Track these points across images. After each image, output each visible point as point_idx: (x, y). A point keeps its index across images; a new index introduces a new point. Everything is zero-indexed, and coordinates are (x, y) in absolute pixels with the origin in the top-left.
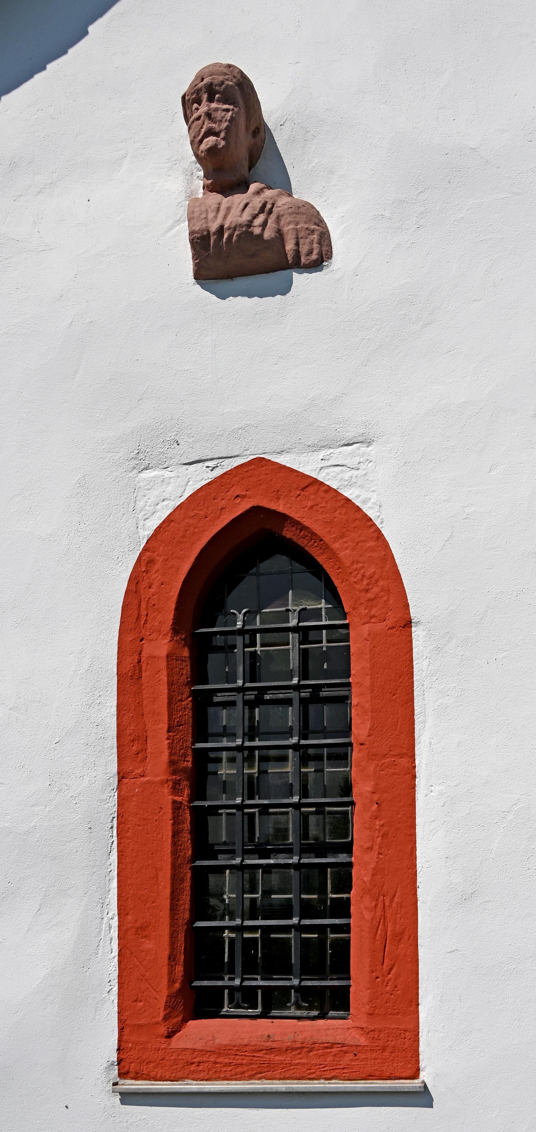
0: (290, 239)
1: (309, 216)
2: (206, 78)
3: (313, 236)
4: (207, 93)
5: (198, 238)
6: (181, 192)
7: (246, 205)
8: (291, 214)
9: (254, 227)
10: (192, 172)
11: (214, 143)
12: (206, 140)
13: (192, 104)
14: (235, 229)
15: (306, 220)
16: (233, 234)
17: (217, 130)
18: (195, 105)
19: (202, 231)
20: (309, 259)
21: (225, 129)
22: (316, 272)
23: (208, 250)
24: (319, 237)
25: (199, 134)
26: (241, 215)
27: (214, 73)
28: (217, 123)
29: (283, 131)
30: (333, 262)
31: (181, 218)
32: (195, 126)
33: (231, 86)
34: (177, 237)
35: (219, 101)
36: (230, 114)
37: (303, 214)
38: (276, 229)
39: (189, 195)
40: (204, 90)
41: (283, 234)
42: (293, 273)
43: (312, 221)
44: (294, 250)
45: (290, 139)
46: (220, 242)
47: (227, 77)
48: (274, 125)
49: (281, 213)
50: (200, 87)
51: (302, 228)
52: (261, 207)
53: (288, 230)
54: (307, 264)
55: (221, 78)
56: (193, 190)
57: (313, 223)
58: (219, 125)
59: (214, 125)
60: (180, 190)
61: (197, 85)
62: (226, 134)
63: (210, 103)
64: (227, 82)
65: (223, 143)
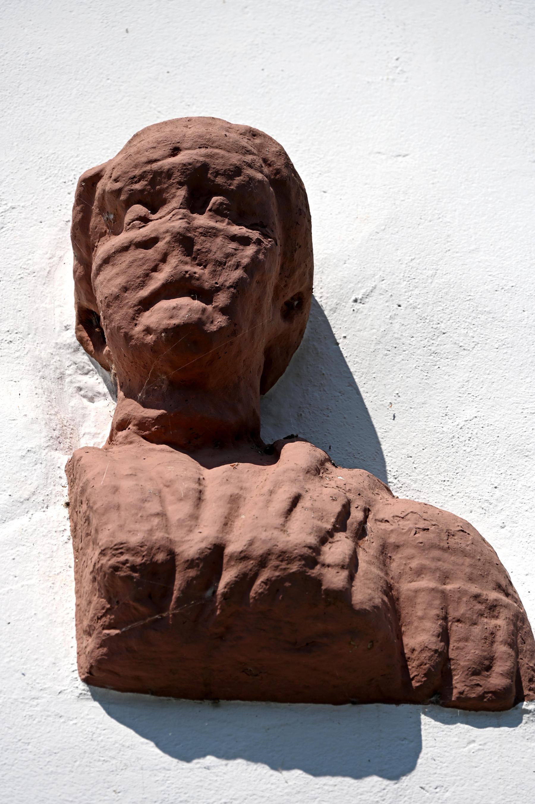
0: (421, 618)
1: (480, 563)
2: (186, 149)
3: (494, 622)
4: (185, 187)
5: (133, 568)
6: (34, 421)
9: (323, 565)
10: (62, 374)
11: (196, 316)
12: (164, 304)
13: (128, 204)
15: (472, 573)
16: (256, 576)
17: (207, 286)
18: (138, 209)
20: (478, 685)
21: (231, 286)
22: (499, 726)
23: (163, 609)
24: (512, 627)
25: (142, 285)
26: (283, 525)
27: (213, 142)
28: (210, 267)
29: (360, 316)
33: (260, 182)
34: (21, 548)
35: (218, 212)
36: (250, 250)
37: (464, 553)
38: (382, 583)
39: (56, 433)
40: (177, 177)
41: (398, 599)
42: (423, 717)
43: (490, 578)
44: (436, 651)
45: (383, 340)
46: (207, 588)
47: (249, 158)
48: (332, 296)
49: (392, 539)
50: (167, 167)
51: (462, 592)
52: (340, 514)
53: (416, 591)
54: (470, 699)
55: (235, 159)
57: (493, 585)
58: (214, 273)
59: (198, 270)
60: (32, 415)
61: (156, 161)
62: (234, 298)
63: (193, 213)
64: (250, 172)
65: (220, 321)
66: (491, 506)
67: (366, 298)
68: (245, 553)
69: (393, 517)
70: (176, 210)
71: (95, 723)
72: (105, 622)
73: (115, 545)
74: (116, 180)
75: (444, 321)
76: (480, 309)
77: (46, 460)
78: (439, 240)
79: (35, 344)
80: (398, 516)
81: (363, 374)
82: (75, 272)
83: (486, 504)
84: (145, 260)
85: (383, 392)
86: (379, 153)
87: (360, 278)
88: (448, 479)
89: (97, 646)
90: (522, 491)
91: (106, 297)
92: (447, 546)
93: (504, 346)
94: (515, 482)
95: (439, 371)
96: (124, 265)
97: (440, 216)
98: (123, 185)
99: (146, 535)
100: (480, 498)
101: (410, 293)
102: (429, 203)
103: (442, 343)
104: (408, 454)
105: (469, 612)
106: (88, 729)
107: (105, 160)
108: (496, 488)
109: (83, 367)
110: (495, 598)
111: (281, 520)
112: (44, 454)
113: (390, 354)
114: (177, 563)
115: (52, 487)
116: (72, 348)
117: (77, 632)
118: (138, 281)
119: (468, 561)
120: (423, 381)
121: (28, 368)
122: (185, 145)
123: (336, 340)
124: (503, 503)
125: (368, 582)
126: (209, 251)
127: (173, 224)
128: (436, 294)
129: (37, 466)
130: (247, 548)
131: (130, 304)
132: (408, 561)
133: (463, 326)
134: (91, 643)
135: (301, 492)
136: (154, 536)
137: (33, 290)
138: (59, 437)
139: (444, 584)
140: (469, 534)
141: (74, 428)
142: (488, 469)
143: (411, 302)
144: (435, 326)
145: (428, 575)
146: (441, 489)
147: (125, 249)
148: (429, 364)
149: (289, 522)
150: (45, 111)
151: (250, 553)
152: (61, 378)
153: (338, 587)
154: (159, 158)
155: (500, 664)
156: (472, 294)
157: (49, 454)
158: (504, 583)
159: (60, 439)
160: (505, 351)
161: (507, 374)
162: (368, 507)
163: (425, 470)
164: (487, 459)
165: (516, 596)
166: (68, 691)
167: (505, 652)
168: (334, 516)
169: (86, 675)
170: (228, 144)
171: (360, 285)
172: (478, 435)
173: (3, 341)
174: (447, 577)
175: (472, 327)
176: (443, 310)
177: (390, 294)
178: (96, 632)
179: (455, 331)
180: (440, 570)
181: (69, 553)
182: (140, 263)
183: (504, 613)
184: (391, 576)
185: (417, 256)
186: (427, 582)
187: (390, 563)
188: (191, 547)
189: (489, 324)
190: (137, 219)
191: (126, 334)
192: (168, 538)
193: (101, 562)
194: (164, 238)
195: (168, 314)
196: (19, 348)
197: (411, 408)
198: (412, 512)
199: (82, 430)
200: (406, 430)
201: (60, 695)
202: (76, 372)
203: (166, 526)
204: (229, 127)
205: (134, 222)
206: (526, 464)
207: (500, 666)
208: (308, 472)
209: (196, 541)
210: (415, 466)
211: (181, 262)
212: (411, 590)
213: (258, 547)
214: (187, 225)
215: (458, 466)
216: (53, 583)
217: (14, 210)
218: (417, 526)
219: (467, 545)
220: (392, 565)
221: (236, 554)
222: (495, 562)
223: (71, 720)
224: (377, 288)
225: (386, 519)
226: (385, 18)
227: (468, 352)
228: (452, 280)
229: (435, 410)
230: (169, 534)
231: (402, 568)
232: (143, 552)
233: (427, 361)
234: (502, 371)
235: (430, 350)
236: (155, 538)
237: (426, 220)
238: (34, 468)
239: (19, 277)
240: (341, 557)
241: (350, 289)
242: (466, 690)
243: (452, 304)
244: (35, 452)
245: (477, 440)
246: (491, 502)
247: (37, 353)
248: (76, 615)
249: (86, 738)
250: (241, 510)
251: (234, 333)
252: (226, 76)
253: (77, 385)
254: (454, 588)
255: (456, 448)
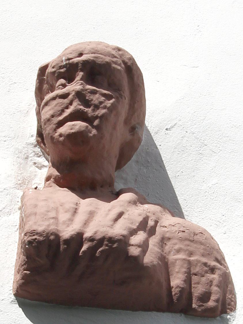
0: (178, 272)
1: (208, 248)
3: (213, 276)
7: (120, 215)
8: (182, 240)
14: (101, 241)
15: (204, 253)
18: (62, 81)
19: (48, 234)
25: (60, 114)
26: (112, 225)
28: (92, 108)
30: (237, 316)
31: (4, 208)
32: (58, 104)
37: (201, 243)
38: (159, 255)
39: (20, 182)
47: (114, 60)
49: (167, 235)
50: (75, 62)
51: (198, 261)
53: (176, 260)
56: (25, 178)
57: (214, 259)
58: (94, 110)
61: (71, 59)
66: (220, 224)
67: (172, 128)
68: (92, 238)
69: (169, 225)
70: (78, 81)
71: (17, 315)
72: (25, 267)
73: (31, 231)
74: (53, 68)
75: (207, 140)
76: (223, 135)
77: (12, 193)
78: (208, 104)
79: (17, 142)
80: (171, 225)
81: (167, 162)
82: (36, 110)
83: (218, 223)
84: (63, 104)
85: (176, 170)
86: (185, 65)
87: (170, 119)
88: (202, 211)
89: (21, 278)
90: (235, 217)
91: (44, 120)
92: (193, 239)
93: (233, 152)
94: (233, 213)
95: (202, 162)
96: (53, 105)
97: (210, 94)
98: (56, 70)
99: (46, 227)
100: (216, 220)
101: (192, 127)
102: (205, 88)
103: (205, 149)
104: (184, 199)
105: (201, 271)
106: (13, 318)
107: (51, 61)
108: (223, 215)
109: (38, 154)
110: (214, 264)
111: (112, 223)
112: (12, 191)
113: (180, 154)
114: (61, 241)
115: (13, 206)
116: (33, 145)
117: (15, 272)
118: (59, 113)
119: (202, 247)
120: (195, 166)
121: (12, 153)
122: (85, 52)
123: (156, 146)
124: (226, 222)
125: (152, 254)
126: (92, 100)
127: (76, 87)
128: (204, 128)
129: (7, 196)
130: (93, 235)
131: (54, 123)
132: (174, 246)
133: (215, 142)
134: (19, 277)
135: (124, 211)
136: (50, 228)
137: (19, 119)
138: (21, 184)
139: (190, 257)
140: (204, 235)
141: (30, 181)
142: (220, 207)
143: (192, 131)
144: (202, 142)
145: (183, 252)
146: (198, 215)
147: (54, 99)
148: (198, 159)
149: (115, 224)
150: (36, 42)
151: (95, 238)
152: (27, 158)
153: (136, 255)
154: (73, 58)
155: (214, 296)
156: (221, 128)
157: (14, 191)
158: (219, 258)
159: (22, 185)
160: (233, 154)
161: (234, 165)
162: (157, 220)
163: (192, 206)
164: (221, 202)
165: (226, 265)
166: (6, 299)
167: (216, 290)
168: (138, 223)
169: (15, 292)
170: (105, 53)
171: (169, 122)
172: (218, 191)
173: (2, 140)
174: (192, 254)
175: (219, 143)
176: (207, 135)
177: (183, 127)
178: (21, 272)
179: (211, 144)
180: (188, 251)
181: (17, 236)
182: (60, 105)
183: (218, 272)
184: (165, 252)
185: (197, 111)
186: (182, 255)
187: (165, 246)
188: (67, 233)
189: (228, 142)
190: (61, 85)
191: (51, 136)
192: (56, 229)
193: (24, 239)
194: (72, 94)
195: (70, 128)
196: (9, 144)
197: (188, 178)
198: (178, 223)
199: (34, 182)
200: (184, 188)
201: (3, 301)
202: (34, 156)
203: (57, 223)
204: (108, 46)
205: (60, 86)
206: (239, 205)
207: (214, 297)
208: (130, 202)
209: (70, 231)
210: (187, 204)
211: (78, 104)
212: (174, 259)
213: (99, 235)
214: (83, 88)
215: (207, 205)
216: (7, 249)
217: (16, 84)
218: (180, 230)
219: (203, 240)
220: (166, 247)
221: (88, 238)
222: (216, 248)
223: (6, 313)
224: (177, 124)
225: (166, 226)
226: (195, 8)
227: (216, 154)
228: (212, 122)
229: (199, 179)
230: (57, 227)
231: (171, 249)
232: (44, 235)
233: (197, 157)
234: (231, 163)
235: (199, 152)
236: (50, 228)
237: (203, 95)
238: (6, 197)
239: (14, 113)
240: (139, 242)
241: (165, 124)
242: (196, 307)
243: (211, 132)
244: (7, 190)
245: (216, 193)
246: (221, 222)
247: (17, 146)
248: (15, 264)
249: (12, 322)
250: (95, 218)
251: (102, 138)
252: (120, 30)
253: (34, 161)
254: (194, 259)
255: (207, 197)
